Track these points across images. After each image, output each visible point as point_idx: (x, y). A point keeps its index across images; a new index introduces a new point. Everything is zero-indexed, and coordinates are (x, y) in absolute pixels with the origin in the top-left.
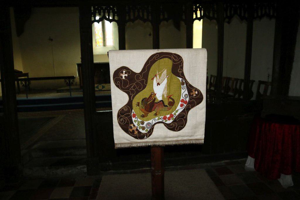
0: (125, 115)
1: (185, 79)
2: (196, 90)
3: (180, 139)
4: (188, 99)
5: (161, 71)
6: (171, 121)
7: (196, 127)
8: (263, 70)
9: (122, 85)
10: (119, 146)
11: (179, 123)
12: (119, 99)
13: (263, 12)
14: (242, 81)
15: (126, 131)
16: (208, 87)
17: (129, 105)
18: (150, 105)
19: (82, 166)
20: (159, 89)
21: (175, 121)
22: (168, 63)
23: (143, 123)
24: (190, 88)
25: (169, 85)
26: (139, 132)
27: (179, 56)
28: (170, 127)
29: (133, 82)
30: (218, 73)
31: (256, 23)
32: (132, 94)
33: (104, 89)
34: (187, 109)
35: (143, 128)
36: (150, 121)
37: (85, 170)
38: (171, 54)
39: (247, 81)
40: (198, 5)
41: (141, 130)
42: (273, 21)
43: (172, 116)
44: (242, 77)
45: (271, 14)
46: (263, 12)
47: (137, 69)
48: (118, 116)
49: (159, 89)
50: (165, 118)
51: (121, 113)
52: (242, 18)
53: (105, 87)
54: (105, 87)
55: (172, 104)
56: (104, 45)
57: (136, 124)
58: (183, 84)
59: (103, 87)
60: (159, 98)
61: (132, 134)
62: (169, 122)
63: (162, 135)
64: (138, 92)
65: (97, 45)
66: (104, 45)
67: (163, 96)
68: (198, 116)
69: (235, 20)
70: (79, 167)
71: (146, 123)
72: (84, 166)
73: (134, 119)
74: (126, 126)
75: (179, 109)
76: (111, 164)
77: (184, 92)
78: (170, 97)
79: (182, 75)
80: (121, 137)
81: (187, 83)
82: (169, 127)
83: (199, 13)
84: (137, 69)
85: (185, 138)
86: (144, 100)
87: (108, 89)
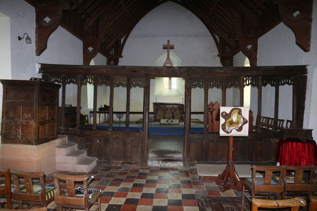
0: (224, 125)
1: (242, 115)
2: (246, 119)
3: (240, 134)
4: (243, 122)
5: (235, 113)
6: (238, 128)
7: (245, 131)
8: (286, 113)
9: (223, 117)
10: (221, 136)
11: (240, 129)
12: (222, 121)
13: (285, 81)
14: (272, 119)
15: (224, 131)
16: (192, 68)
17: (225, 122)
18: (231, 123)
19: (180, 162)
20: (234, 118)
21: (239, 128)
22: (237, 111)
23: (229, 129)
24: (244, 119)
25: (237, 117)
26: (228, 131)
27: (240, 109)
28: (237, 130)
29: (227, 116)
30: (104, 113)
31: (281, 87)
32: (226, 120)
33: (172, 123)
34: (243, 125)
35: (229, 130)
36: (231, 128)
37: (182, 165)
38: (238, 108)
39: (276, 119)
40: (247, 78)
41: (228, 131)
42: (291, 86)
43: (238, 127)
44: (273, 117)
45: (290, 82)
46: (285, 81)
47: (228, 112)
48: (222, 126)
49: (234, 118)
50: (236, 127)
51: (223, 125)
52: (272, 85)
53: (166, 121)
54: (166, 121)
55: (238, 123)
56: (170, 88)
57: (227, 129)
58: (241, 117)
59: (172, 122)
60: (234, 121)
61: (225, 132)
62: (237, 129)
63: (235, 133)
64: (228, 119)
65: (164, 88)
66: (170, 88)
67: (235, 121)
68: (246, 127)
69: (269, 85)
70: (178, 163)
71: (230, 128)
72: (181, 162)
73: (226, 127)
74: (224, 129)
75: (240, 125)
76: (196, 162)
77: (242, 119)
78: (237, 121)
79: (241, 115)
80: (222, 133)
81: (243, 117)
82: (237, 130)
83: (247, 82)
84: (228, 112)
85: (242, 134)
86: (230, 122)
87: (175, 123)
